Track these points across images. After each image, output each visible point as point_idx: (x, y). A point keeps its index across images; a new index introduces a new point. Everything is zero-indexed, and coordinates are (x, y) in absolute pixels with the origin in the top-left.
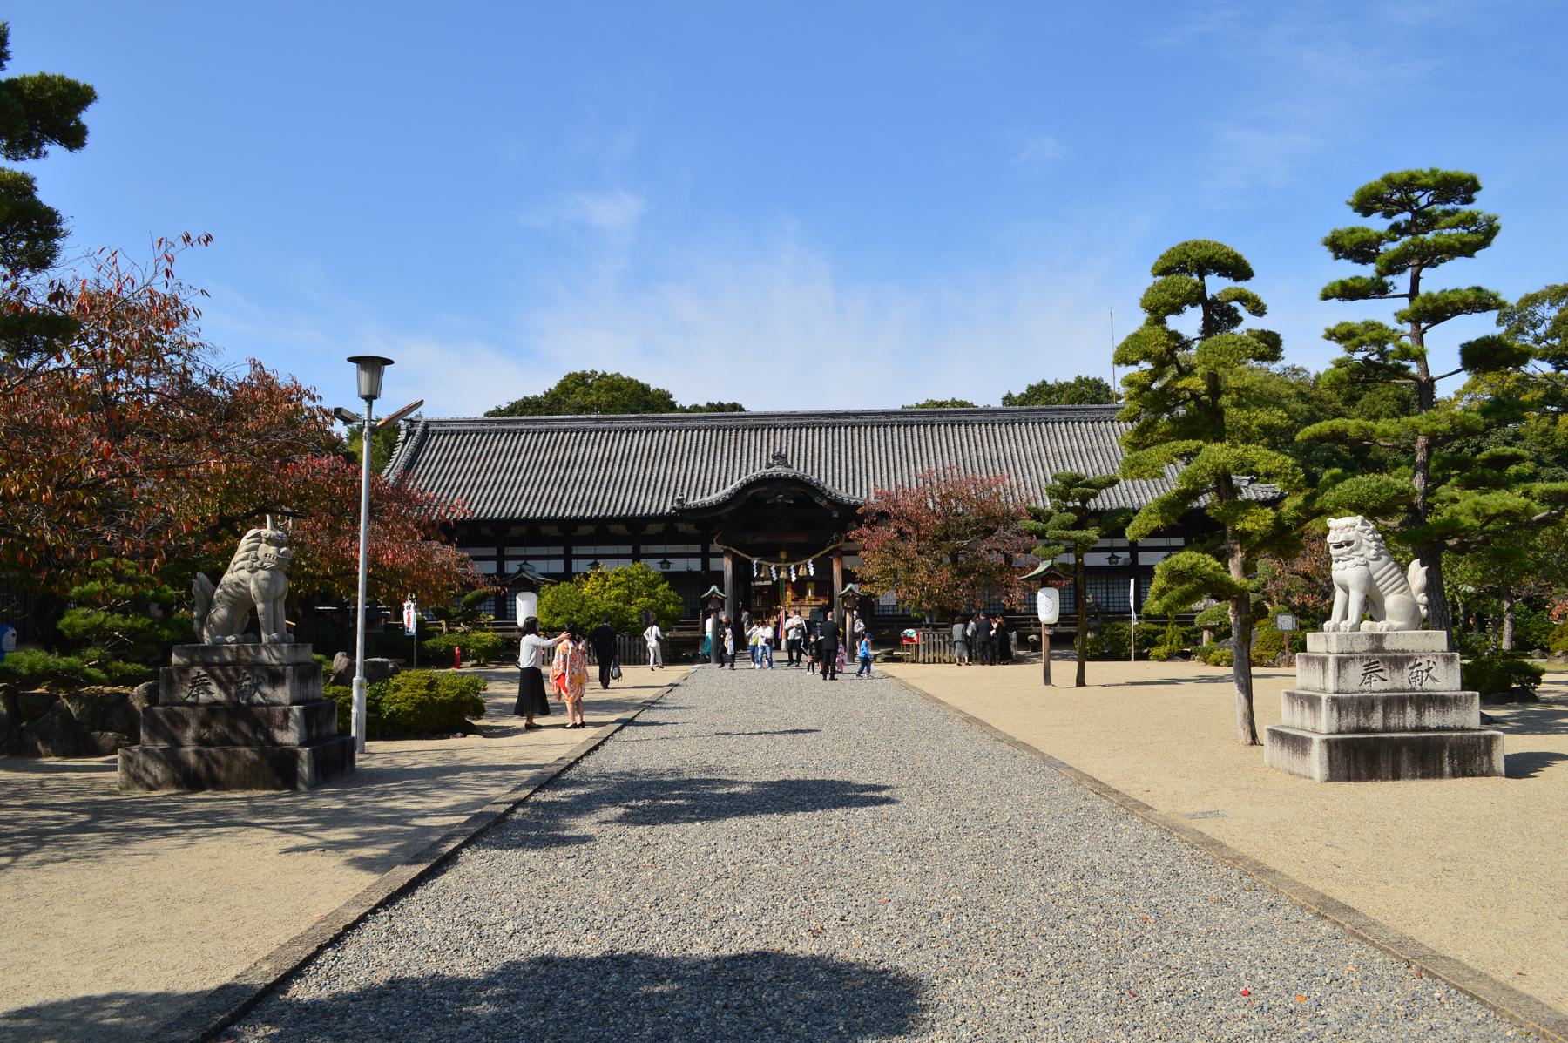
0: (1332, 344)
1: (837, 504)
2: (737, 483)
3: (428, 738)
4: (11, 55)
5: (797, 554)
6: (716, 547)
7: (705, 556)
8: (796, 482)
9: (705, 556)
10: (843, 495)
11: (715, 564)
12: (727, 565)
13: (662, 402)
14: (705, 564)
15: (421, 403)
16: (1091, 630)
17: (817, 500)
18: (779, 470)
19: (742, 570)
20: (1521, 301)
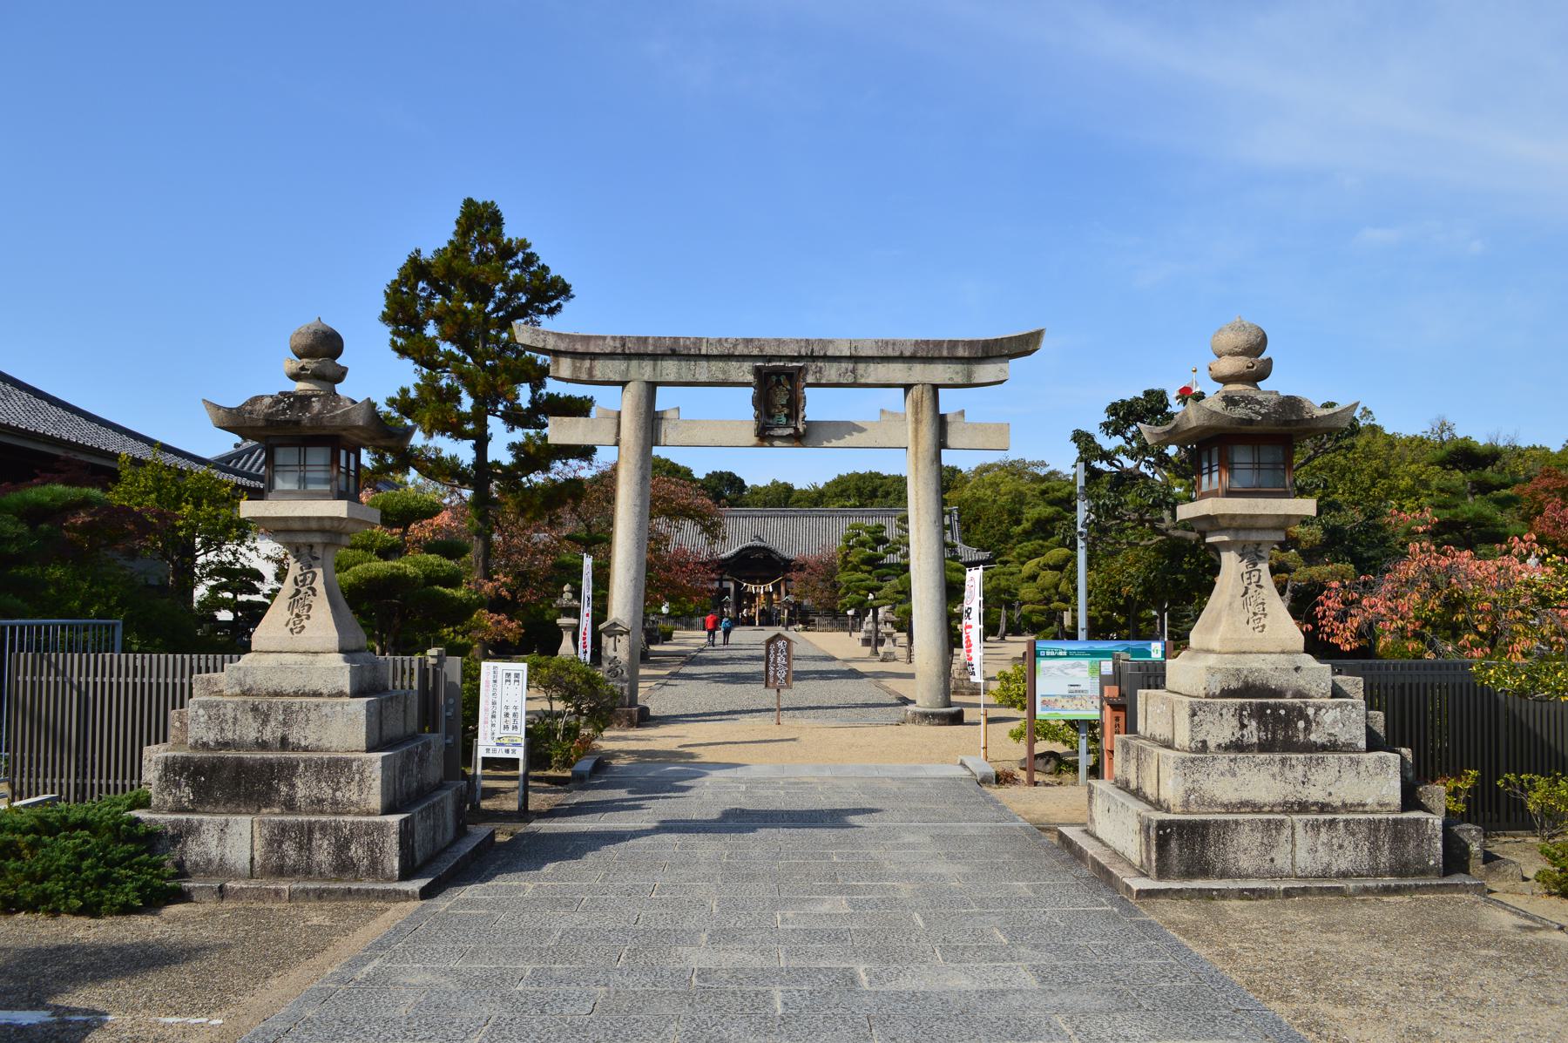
0: (1073, 452)
1: (783, 559)
2: (740, 546)
3: (52, 454)
4: (453, 454)
5: (764, 581)
6: (726, 577)
7: (721, 581)
8: (764, 548)
9: (721, 581)
10: (786, 555)
11: (725, 585)
12: (732, 586)
13: (1229, 354)
14: (721, 585)
15: (1024, 345)
16: (849, 609)
17: (774, 556)
18: (757, 543)
19: (738, 586)
20: (978, 468)
